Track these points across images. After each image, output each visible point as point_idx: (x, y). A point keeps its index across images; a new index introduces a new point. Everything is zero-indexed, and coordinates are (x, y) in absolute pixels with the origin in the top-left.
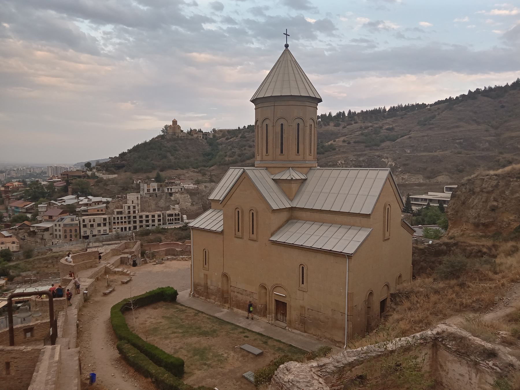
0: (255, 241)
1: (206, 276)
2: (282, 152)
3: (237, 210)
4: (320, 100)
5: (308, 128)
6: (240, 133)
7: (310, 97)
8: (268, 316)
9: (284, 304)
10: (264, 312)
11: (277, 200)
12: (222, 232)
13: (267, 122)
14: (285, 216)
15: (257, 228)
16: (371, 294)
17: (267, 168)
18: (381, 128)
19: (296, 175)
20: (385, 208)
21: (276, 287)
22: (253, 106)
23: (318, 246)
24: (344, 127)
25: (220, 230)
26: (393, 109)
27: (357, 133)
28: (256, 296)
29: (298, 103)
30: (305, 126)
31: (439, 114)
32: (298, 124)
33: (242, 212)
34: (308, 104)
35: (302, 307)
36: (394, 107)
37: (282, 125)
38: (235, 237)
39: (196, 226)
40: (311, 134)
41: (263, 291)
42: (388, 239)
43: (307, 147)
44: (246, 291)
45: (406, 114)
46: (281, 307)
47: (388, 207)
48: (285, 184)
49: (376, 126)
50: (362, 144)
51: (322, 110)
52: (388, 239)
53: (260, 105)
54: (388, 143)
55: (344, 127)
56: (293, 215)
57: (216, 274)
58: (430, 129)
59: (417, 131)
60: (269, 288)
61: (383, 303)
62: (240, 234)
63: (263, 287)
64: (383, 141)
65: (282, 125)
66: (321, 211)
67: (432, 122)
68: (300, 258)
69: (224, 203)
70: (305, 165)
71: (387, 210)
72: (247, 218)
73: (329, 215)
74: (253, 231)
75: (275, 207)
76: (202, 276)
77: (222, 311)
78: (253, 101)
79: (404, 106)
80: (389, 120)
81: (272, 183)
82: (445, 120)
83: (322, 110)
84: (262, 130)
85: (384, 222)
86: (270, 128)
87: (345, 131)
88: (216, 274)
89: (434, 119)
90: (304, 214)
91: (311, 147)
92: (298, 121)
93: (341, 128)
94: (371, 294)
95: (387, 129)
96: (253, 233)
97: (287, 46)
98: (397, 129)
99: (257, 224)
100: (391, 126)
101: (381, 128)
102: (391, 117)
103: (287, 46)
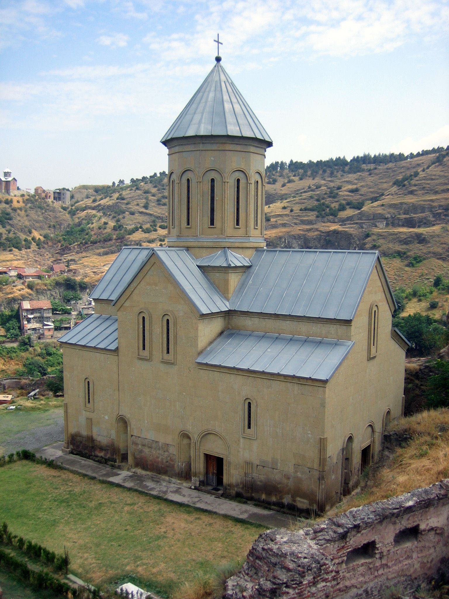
0: (172, 364)
1: (90, 420)
2: (212, 223)
3: (142, 315)
4: (269, 144)
5: (252, 187)
6: (114, 191)
7: (255, 139)
8: (193, 478)
9: (219, 461)
10: (186, 475)
11: (206, 301)
12: (117, 350)
13: (188, 175)
14: (217, 325)
15: (175, 343)
16: (350, 439)
17: (188, 249)
18: (339, 188)
19: (237, 259)
20: (371, 309)
21: (206, 435)
22: (165, 150)
23: (288, 371)
24: (284, 185)
25: (113, 347)
26: (356, 160)
27: (305, 195)
28: (172, 450)
29: (238, 148)
30: (248, 183)
31: (423, 170)
32: (238, 180)
33: (151, 317)
34: (252, 149)
35: (248, 463)
36: (358, 157)
37: (213, 180)
38: (162, 362)
39: (73, 341)
40: (257, 195)
41: (186, 441)
42: (374, 357)
43: (252, 216)
44: (157, 442)
45: (375, 169)
46: (215, 464)
47: (375, 308)
48: (217, 275)
49: (332, 185)
50: (312, 213)
51: (272, 156)
52: (374, 357)
53: (177, 149)
54: (349, 212)
55: (284, 185)
56: (232, 324)
57: (106, 417)
58: (412, 192)
59: (392, 195)
60: (195, 437)
61: (366, 453)
62: (146, 353)
63: (185, 436)
64: (342, 208)
65: (213, 180)
66: (276, 316)
67: (413, 182)
68: (245, 388)
69: (119, 304)
70: (248, 245)
71: (373, 315)
72: (157, 331)
73: (288, 322)
74: (144, 346)
75: (205, 310)
76: (82, 420)
77: (119, 474)
78: (165, 143)
79: (373, 156)
80: (352, 177)
81: (197, 271)
82: (432, 179)
83: (272, 156)
84: (180, 189)
85: (370, 331)
86: (193, 185)
87: (284, 190)
88: (106, 417)
89: (417, 178)
90: (248, 322)
91: (257, 217)
92: (213, 175)
93: (278, 185)
94: (350, 439)
95: (352, 191)
96: (144, 349)
97: (218, 59)
98: (363, 190)
99: (175, 337)
100: (354, 187)
101: (339, 188)
102: (355, 173)
103: (218, 59)
